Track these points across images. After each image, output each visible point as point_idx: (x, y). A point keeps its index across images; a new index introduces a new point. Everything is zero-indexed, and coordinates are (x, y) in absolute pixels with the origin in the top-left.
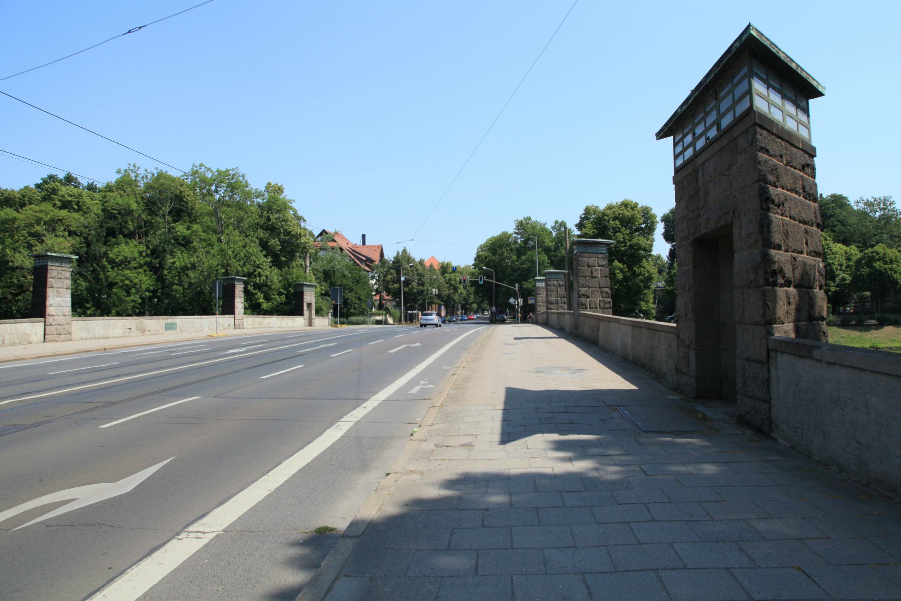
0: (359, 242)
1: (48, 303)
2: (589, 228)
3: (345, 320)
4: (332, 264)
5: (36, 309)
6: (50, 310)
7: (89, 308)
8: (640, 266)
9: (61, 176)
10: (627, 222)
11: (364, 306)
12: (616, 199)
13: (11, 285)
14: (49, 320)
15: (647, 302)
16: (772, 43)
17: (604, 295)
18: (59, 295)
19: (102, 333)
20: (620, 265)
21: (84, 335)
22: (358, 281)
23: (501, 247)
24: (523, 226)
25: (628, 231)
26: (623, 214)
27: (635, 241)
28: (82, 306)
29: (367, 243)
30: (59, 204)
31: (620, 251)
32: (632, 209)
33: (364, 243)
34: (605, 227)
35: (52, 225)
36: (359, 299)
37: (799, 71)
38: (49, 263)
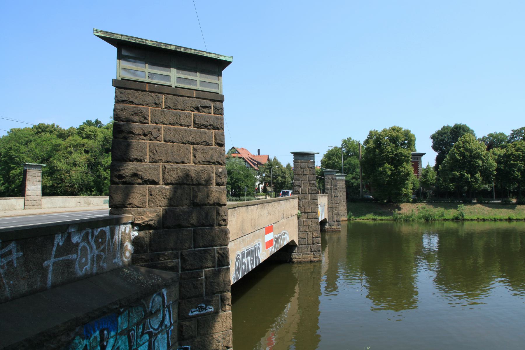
0: (256, 153)
1: (26, 189)
2: (371, 145)
3: (238, 198)
4: (232, 167)
5: (19, 191)
6: (27, 193)
7: (93, 191)
8: (402, 167)
9: (93, 121)
10: (394, 140)
11: (250, 190)
12: (388, 126)
13: (57, 179)
14: (27, 198)
15: (407, 188)
16: (122, 35)
17: (311, 185)
18: (34, 185)
19: (61, 205)
20: (389, 166)
21: (50, 206)
22: (247, 176)
23: (333, 155)
24: (346, 143)
25: (394, 146)
26: (391, 135)
27: (399, 151)
28: (48, 191)
29: (261, 154)
30: (85, 136)
31: (389, 157)
32: (398, 131)
33: (259, 154)
34: (380, 143)
35: (76, 147)
36: (248, 186)
37: (188, 51)
38: (28, 169)
